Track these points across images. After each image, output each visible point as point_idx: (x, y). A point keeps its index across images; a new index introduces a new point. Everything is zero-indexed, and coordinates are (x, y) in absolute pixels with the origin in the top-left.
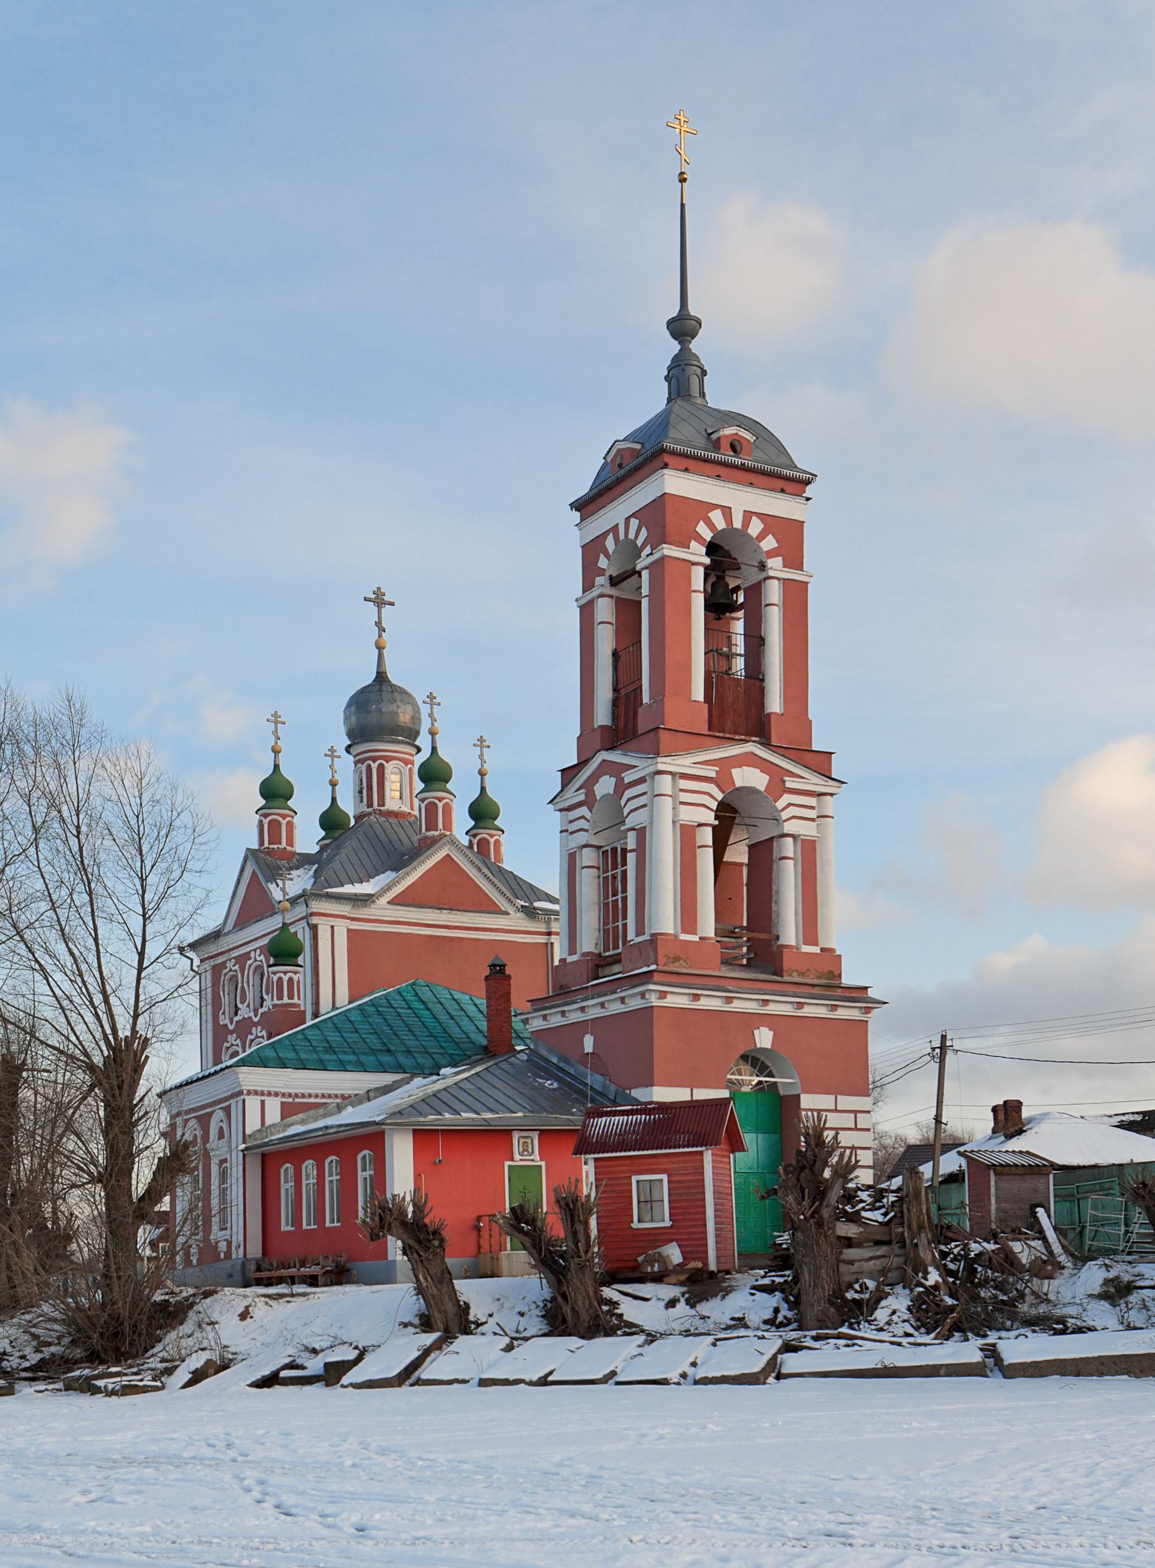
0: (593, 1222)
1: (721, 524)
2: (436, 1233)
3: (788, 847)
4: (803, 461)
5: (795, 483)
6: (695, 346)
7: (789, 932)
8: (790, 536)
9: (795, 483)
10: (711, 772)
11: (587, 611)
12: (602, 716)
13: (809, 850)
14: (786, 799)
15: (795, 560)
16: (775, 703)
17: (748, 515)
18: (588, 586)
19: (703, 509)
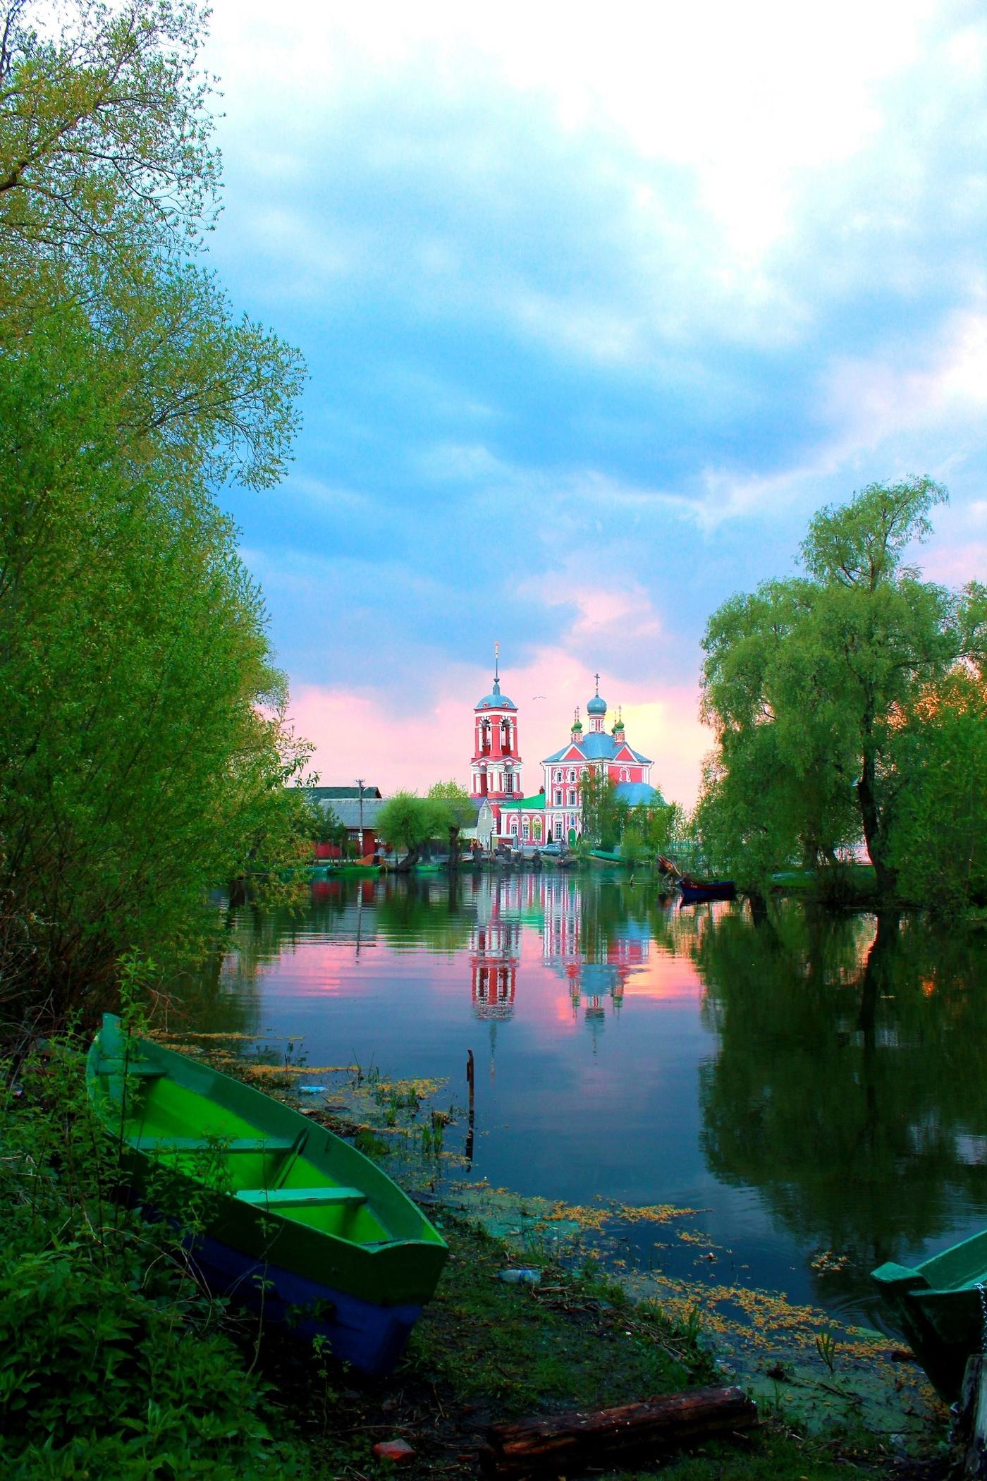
7: (515, 790)
8: (514, 719)
11: (477, 730)
12: (481, 749)
16: (512, 748)
19: (500, 717)
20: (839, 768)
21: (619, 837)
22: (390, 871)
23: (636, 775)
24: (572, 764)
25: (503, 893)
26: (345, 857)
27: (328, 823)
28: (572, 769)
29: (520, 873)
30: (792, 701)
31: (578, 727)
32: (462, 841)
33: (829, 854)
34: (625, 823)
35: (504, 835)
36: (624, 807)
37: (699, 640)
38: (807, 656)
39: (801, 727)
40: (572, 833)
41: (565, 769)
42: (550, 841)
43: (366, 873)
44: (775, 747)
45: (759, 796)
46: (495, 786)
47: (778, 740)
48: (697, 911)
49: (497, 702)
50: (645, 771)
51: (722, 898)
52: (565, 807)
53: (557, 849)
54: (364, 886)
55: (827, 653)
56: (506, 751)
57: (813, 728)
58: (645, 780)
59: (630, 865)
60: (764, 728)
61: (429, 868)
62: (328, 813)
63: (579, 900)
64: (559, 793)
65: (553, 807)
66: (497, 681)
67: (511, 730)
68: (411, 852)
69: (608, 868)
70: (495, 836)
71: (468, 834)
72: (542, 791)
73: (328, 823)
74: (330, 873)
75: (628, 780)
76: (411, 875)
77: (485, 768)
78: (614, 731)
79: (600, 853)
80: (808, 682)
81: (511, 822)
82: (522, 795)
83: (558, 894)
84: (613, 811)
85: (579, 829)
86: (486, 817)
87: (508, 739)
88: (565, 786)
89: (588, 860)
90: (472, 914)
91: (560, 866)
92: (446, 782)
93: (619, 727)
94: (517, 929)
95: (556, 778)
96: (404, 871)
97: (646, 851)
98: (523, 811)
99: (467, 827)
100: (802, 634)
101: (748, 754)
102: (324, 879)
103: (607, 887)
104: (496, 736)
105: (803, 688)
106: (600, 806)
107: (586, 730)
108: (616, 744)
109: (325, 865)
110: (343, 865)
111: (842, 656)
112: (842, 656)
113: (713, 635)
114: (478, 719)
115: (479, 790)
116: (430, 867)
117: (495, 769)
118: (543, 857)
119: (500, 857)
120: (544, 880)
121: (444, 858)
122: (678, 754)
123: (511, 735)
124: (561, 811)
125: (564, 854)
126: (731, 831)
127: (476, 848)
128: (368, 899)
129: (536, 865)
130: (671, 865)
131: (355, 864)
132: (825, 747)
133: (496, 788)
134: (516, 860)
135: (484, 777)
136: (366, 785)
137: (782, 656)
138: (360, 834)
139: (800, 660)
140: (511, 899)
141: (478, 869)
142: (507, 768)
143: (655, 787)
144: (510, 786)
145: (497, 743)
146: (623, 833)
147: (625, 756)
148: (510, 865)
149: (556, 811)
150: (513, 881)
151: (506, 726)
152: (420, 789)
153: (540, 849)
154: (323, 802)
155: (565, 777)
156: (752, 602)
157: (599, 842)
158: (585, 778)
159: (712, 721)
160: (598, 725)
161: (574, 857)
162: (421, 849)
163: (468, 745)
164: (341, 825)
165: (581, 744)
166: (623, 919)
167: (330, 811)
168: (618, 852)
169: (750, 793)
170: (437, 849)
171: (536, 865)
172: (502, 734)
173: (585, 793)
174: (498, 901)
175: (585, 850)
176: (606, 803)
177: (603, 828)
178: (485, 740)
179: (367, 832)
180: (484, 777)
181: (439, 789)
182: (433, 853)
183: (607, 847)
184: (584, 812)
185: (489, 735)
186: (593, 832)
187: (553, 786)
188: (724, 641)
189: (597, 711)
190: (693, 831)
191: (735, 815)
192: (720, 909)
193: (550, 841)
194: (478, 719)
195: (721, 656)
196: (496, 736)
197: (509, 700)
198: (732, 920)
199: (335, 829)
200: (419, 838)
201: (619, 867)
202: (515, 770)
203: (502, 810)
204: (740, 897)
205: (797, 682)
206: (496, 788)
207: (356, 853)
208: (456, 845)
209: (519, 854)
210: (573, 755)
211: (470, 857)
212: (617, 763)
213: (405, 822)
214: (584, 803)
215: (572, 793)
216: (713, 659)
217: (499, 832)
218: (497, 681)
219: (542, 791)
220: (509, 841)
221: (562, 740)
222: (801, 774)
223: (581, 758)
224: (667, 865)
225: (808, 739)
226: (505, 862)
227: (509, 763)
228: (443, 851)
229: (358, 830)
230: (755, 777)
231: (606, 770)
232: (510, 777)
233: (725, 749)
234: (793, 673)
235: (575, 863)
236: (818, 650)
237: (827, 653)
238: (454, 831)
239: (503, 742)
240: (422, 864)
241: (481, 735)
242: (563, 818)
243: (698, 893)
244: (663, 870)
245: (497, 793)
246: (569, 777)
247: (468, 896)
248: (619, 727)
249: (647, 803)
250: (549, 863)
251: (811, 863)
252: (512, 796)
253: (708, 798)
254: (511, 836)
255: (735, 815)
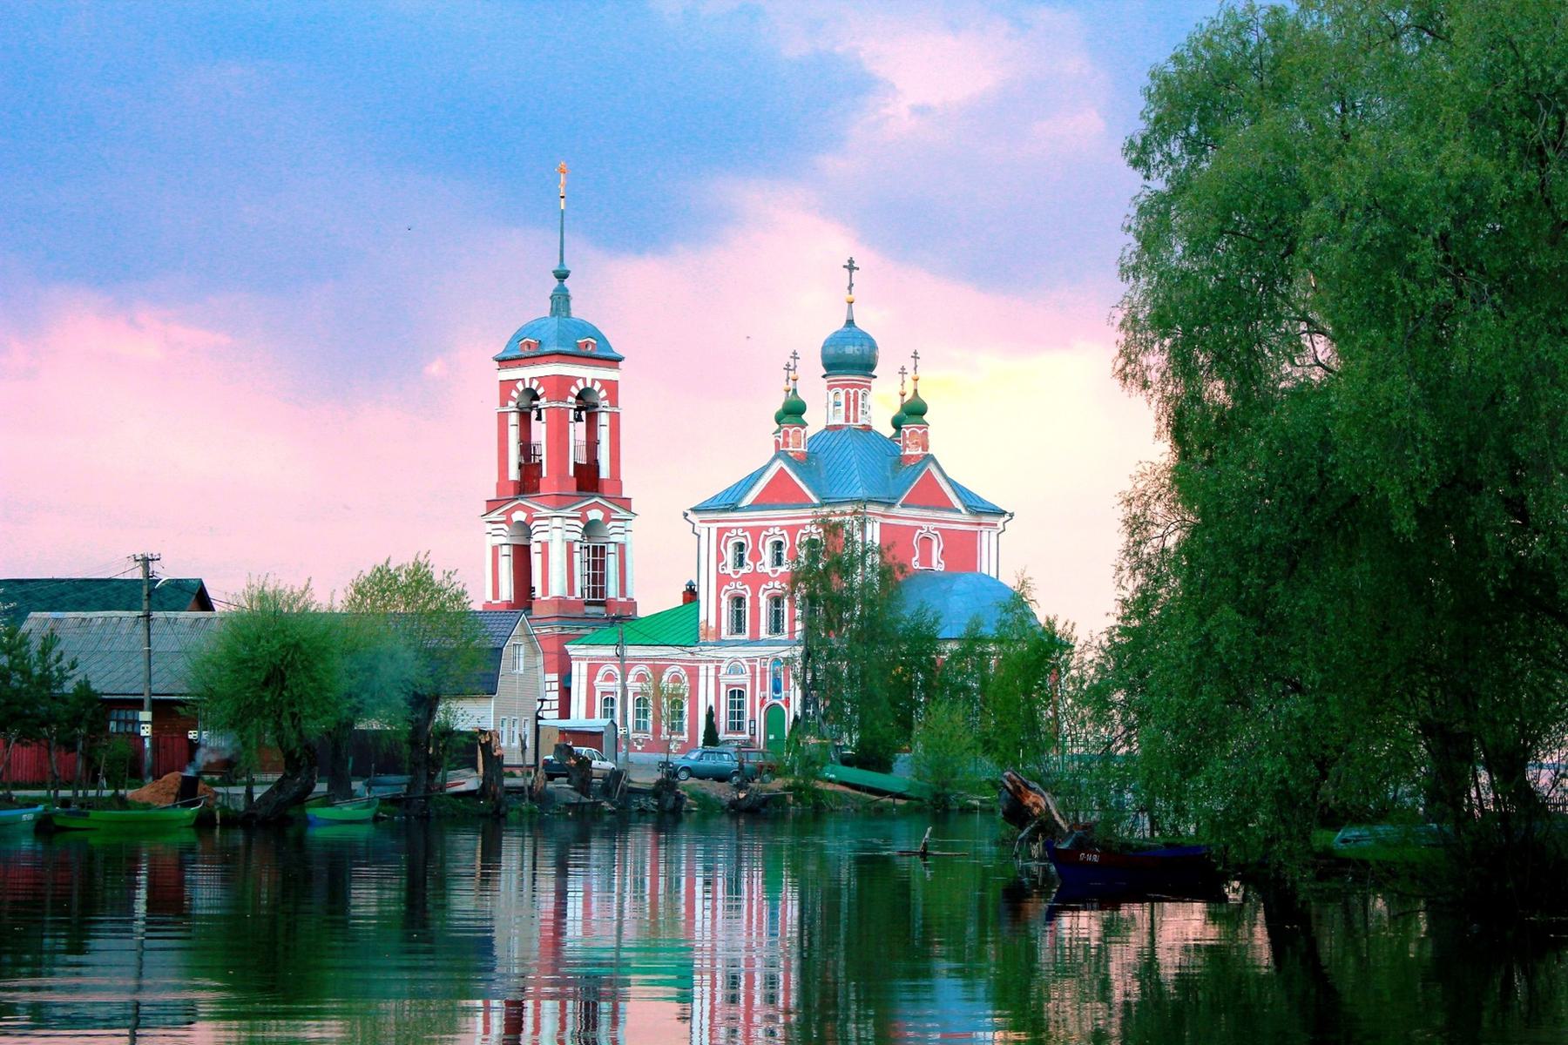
0: (1424, 926)
1: (582, 387)
2: (79, 949)
3: (611, 548)
4: (618, 350)
5: (614, 361)
6: (567, 282)
7: (612, 591)
8: (612, 387)
9: (614, 361)
10: (578, 514)
11: (503, 417)
12: (514, 474)
13: (622, 548)
14: (611, 524)
15: (614, 403)
16: (604, 473)
17: (593, 381)
18: (504, 404)
19: (571, 380)
20: (1516, 506)
21: (906, 725)
22: (230, 821)
23: (962, 549)
24: (777, 521)
25: (575, 886)
26: (94, 782)
27: (45, 680)
28: (776, 534)
29: (618, 827)
30: (1381, 310)
31: (793, 412)
32: (448, 733)
33: (1511, 766)
34: (927, 687)
35: (578, 718)
36: (924, 640)
37: (1121, 142)
38: (1423, 174)
39: (1402, 387)
40: (774, 714)
41: (756, 532)
42: (711, 736)
43: (160, 827)
44: (1326, 445)
45: (1279, 587)
46: (556, 578)
47: (1336, 431)
48: (1111, 930)
49: (561, 339)
50: (987, 540)
51: (1182, 893)
52: (755, 641)
53: (727, 761)
54: (153, 860)
55: (1487, 167)
56: (587, 479)
57: (1435, 392)
58: (986, 566)
59: (939, 808)
60: (1302, 393)
61: (340, 816)
62: (45, 652)
63: (792, 911)
64: (739, 601)
65: (720, 643)
66: (562, 276)
67: (604, 419)
68: (292, 763)
69: (876, 810)
70: (551, 718)
71: (468, 715)
72: (691, 595)
73: (45, 680)
74: (44, 827)
75: (938, 564)
76: (291, 832)
77: (525, 529)
78: (897, 424)
79: (855, 774)
80: (1426, 254)
81: (601, 685)
82: (632, 605)
83: (734, 887)
84: (886, 649)
85: (795, 707)
86: (521, 664)
87: (592, 444)
88: (756, 580)
89: (817, 794)
90: (474, 954)
91: (736, 809)
92: (401, 559)
93: (913, 411)
94: (615, 999)
95: (729, 556)
96: (276, 823)
97: (986, 768)
98: (631, 651)
99: (460, 695)
100: (1421, 114)
101: (1248, 469)
102: (26, 843)
103: (871, 865)
104: (559, 437)
105: (1410, 271)
106: (857, 637)
107: (816, 420)
108: (899, 462)
109: (31, 803)
110: (88, 804)
111: (1529, 177)
112: (1529, 177)
113: (1162, 128)
114: (506, 386)
115: (507, 592)
116: (347, 810)
117: (556, 536)
118: (686, 783)
119: (561, 785)
120: (688, 851)
121: (395, 784)
122: (1061, 480)
123: (604, 434)
124: (743, 653)
125: (745, 776)
126: (1194, 691)
127: (477, 748)
128: (169, 903)
129: (666, 808)
130: (1040, 801)
131: (123, 803)
132: (1474, 446)
133: (557, 587)
134: (606, 790)
135: (522, 556)
136: (165, 572)
137: (1350, 180)
138: (145, 716)
139: (1400, 191)
140: (598, 905)
141: (492, 814)
142: (590, 528)
143: (1009, 580)
144: (597, 578)
145: (563, 464)
146: (919, 717)
147: (931, 496)
148: (585, 805)
149: (726, 653)
150: (597, 850)
151: (587, 405)
152: (326, 585)
153: (677, 760)
154: (37, 621)
155: (756, 556)
156: (1276, 31)
157: (849, 741)
158: (813, 556)
159: (1153, 376)
160: (852, 404)
161: (777, 784)
162: (339, 756)
163: (482, 467)
164: (84, 686)
165: (804, 463)
166: (920, 972)
167: (50, 641)
168: (902, 774)
169: (1252, 578)
170: (374, 757)
171: (666, 808)
172: (577, 432)
173: (811, 599)
174: (560, 912)
175: (810, 764)
176: (873, 631)
177: (866, 700)
178: (526, 448)
179: (164, 709)
180: (522, 556)
181: (382, 582)
182: (360, 773)
183: (872, 757)
184: (808, 655)
185: (539, 432)
186: (835, 713)
187: (723, 579)
188: (1195, 147)
189: (850, 361)
190: (1097, 697)
191: (1207, 642)
192: (1184, 926)
193: (711, 736)
194: (506, 386)
195: (1180, 186)
196: (559, 437)
197: (601, 338)
198: (1219, 959)
199: (63, 699)
200: (315, 728)
201: (905, 813)
202: (613, 534)
203: (571, 649)
204: (1234, 891)
205: (1392, 252)
206: (557, 587)
207: (133, 770)
208: (434, 748)
209: (616, 775)
210: (779, 494)
211: (469, 781)
212: (903, 515)
213: (276, 677)
214: (809, 629)
215: (777, 601)
216: (1161, 198)
217: (565, 712)
218: (562, 276)
219: (691, 595)
220: (592, 738)
221: (751, 448)
222: (1405, 525)
223: (804, 503)
224: (1030, 799)
225: (1423, 419)
226: (574, 797)
227: (595, 514)
228: (391, 765)
229: (138, 704)
230: (1260, 524)
231: (873, 534)
232: (597, 556)
233: (1184, 455)
234: (1382, 226)
235: (775, 800)
236: (1458, 158)
237: (1487, 167)
238: (425, 703)
239: (576, 454)
240: (327, 801)
241: (513, 434)
242: (745, 680)
243: (1118, 876)
244: (1017, 813)
245: (560, 602)
246: (767, 555)
247: (464, 901)
248: (913, 411)
249: (988, 631)
250: (705, 802)
251: (1448, 789)
252: (602, 611)
253: (1141, 605)
254: (599, 723)
255: (1207, 642)
